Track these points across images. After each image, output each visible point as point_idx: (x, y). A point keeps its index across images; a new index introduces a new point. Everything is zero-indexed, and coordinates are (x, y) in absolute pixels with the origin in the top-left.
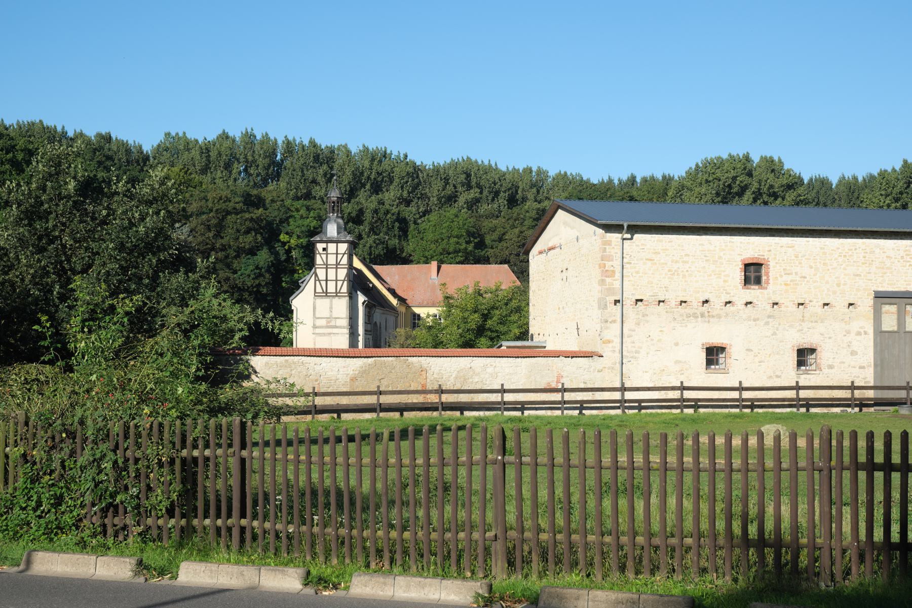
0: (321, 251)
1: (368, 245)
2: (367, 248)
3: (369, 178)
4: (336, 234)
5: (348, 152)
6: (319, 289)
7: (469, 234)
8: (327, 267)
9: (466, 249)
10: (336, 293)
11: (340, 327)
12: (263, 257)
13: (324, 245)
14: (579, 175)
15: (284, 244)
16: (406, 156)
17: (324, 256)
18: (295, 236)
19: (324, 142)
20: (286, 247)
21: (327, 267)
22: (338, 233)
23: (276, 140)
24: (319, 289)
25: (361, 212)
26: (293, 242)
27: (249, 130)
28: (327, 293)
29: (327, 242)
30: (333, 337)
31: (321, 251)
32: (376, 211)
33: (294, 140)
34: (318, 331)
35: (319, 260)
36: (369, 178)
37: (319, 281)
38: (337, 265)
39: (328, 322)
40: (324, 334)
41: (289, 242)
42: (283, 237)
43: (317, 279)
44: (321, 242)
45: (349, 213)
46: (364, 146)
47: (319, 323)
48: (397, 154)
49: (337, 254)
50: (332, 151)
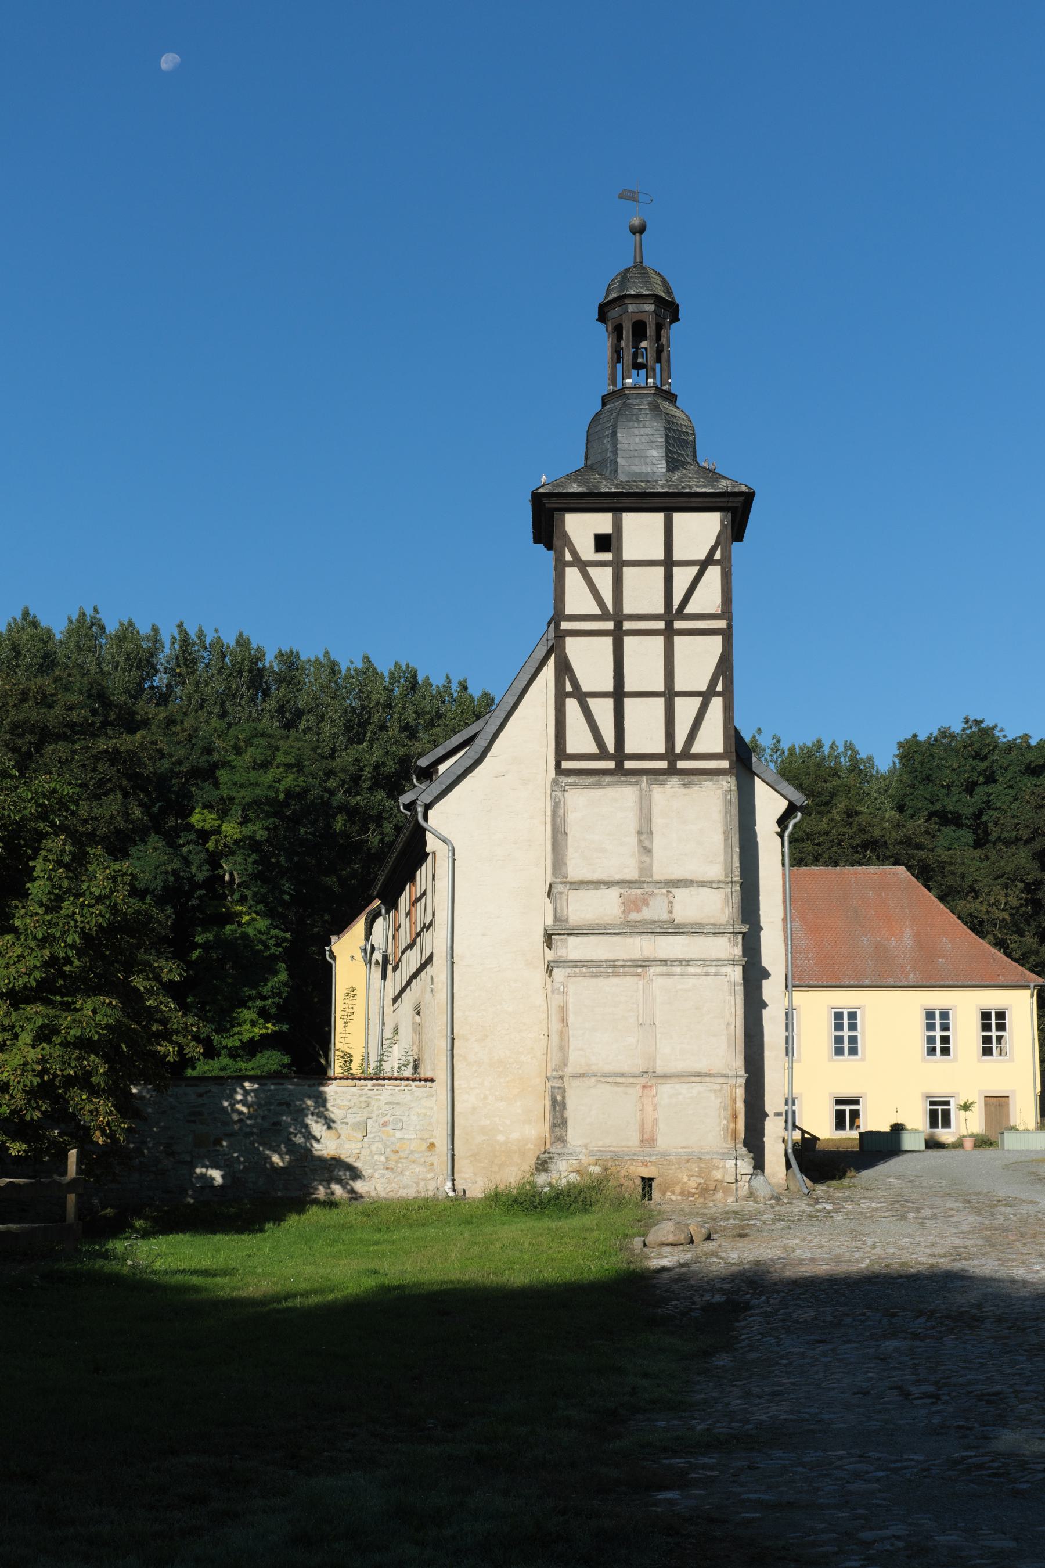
0: (586, 550)
4: (662, 467)
5: (333, 667)
6: (580, 740)
8: (618, 626)
10: (670, 755)
11: (698, 930)
12: (149, 861)
13: (603, 522)
14: (849, 746)
15: (204, 835)
17: (603, 578)
18: (237, 813)
19: (271, 647)
20: (210, 845)
21: (618, 626)
23: (155, 630)
24: (580, 740)
26: (230, 829)
27: (89, 612)
28: (620, 755)
30: (659, 981)
31: (586, 550)
33: (201, 635)
34: (575, 948)
38: (671, 621)
39: (631, 905)
40: (610, 967)
41: (217, 831)
42: (199, 818)
44: (590, 502)
45: (377, 767)
46: (367, 659)
47: (582, 907)
49: (669, 563)
50: (290, 661)
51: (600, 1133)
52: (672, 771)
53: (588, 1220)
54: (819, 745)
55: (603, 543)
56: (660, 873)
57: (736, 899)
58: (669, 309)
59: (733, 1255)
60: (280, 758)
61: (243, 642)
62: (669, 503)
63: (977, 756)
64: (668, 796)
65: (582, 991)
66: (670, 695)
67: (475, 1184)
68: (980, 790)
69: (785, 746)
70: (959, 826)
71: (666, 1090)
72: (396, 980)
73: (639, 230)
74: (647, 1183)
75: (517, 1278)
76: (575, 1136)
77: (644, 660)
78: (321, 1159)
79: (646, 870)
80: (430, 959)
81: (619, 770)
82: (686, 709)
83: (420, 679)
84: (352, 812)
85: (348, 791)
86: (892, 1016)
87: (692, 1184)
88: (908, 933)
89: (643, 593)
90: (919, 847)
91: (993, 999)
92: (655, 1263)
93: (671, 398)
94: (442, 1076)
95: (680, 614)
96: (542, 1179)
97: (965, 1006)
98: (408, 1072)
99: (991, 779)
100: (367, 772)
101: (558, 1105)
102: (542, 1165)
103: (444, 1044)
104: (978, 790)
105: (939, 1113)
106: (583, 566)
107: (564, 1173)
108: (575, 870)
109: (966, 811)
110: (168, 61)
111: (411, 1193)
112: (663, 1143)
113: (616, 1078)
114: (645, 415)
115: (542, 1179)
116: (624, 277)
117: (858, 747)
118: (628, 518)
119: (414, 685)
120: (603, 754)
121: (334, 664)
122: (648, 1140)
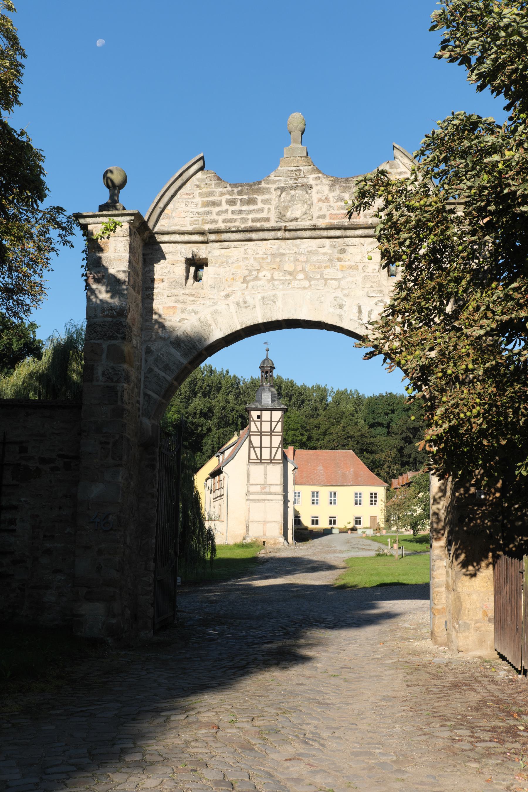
0: (255, 418)
1: (217, 436)
2: (216, 439)
3: (201, 387)
4: (270, 402)
6: (253, 456)
7: (303, 427)
8: (261, 434)
9: (301, 440)
10: (270, 459)
11: (275, 494)
13: (258, 413)
14: (356, 391)
16: (228, 372)
17: (258, 424)
21: (261, 434)
24: (253, 456)
25: (210, 410)
28: (261, 459)
29: (261, 410)
32: (224, 408)
34: (251, 497)
35: (253, 428)
36: (201, 387)
37: (254, 448)
38: (271, 433)
39: (263, 489)
40: (258, 501)
43: (251, 445)
44: (256, 409)
45: (201, 410)
47: (253, 489)
48: (220, 370)
49: (271, 421)
51: (256, 533)
52: (271, 463)
53: (252, 549)
54: (346, 390)
55: (259, 417)
56: (268, 483)
60: (173, 409)
62: (272, 410)
63: (389, 405)
64: (270, 467)
65: (252, 505)
67: (231, 542)
68: (390, 415)
69: (335, 390)
70: (383, 427)
71: (268, 525)
73: (268, 351)
74: (264, 542)
75: (238, 557)
76: (251, 533)
79: (265, 482)
80: (223, 495)
81: (261, 462)
82: (274, 451)
83: (213, 369)
84: (193, 423)
85: (193, 417)
86: (346, 494)
87: (273, 543)
88: (352, 470)
89: (266, 427)
90: (366, 437)
91: (374, 490)
92: (260, 556)
94: (225, 520)
95: (273, 432)
96: (244, 541)
97: (366, 491)
99: (393, 411)
100: (198, 412)
101: (247, 527)
102: (244, 539)
103: (226, 514)
104: (389, 415)
105: (358, 521)
106: (254, 421)
107: (248, 540)
108: (252, 482)
109: (384, 422)
110: (100, 43)
114: (268, 391)
115: (244, 541)
116: (264, 361)
117: (359, 392)
120: (258, 459)
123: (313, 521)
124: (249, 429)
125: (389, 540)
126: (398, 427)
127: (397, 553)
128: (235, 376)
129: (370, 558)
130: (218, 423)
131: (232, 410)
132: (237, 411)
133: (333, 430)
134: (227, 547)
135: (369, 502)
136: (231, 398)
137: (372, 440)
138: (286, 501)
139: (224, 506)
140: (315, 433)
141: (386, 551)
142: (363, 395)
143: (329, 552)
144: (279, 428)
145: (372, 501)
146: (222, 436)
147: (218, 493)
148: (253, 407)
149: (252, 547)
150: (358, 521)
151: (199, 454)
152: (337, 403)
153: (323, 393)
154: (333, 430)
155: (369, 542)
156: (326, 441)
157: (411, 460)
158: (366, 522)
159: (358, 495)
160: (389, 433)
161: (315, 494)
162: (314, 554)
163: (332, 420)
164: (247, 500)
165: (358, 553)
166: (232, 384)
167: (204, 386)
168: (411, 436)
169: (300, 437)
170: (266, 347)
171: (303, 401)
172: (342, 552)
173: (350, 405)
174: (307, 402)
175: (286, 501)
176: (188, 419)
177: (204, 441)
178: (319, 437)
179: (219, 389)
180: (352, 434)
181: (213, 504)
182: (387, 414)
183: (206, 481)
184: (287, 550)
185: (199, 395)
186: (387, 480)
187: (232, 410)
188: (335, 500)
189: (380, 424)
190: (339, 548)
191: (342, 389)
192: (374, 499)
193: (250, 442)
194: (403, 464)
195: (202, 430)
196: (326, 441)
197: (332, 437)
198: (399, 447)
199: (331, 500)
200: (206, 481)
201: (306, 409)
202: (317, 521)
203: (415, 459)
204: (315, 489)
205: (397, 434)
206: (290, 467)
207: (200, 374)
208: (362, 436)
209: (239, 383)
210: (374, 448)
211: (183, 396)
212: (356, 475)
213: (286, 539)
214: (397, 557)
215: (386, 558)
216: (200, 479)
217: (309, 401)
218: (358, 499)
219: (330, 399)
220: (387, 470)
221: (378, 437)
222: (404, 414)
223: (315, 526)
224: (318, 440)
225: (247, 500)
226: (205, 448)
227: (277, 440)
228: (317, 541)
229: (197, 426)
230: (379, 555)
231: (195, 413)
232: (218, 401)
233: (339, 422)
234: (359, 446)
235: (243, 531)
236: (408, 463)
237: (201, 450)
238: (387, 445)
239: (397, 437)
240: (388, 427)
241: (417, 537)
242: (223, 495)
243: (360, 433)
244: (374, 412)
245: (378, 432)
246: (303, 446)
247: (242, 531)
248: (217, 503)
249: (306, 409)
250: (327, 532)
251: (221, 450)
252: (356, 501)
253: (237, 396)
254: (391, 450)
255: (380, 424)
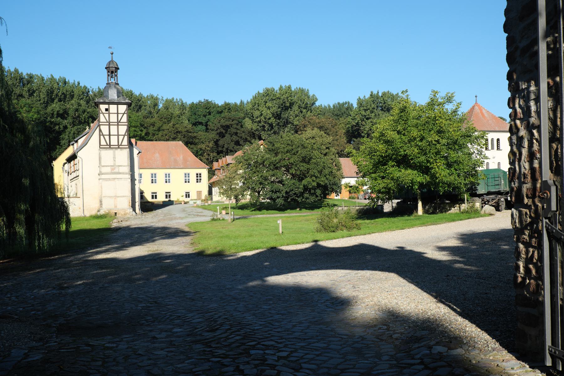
0: (104, 111)
1: (72, 132)
3: (57, 95)
6: (103, 143)
8: (109, 124)
9: (141, 135)
10: (118, 145)
11: (123, 173)
14: (181, 100)
17: (107, 116)
21: (109, 124)
22: (118, 97)
28: (110, 145)
29: (109, 103)
32: (77, 110)
34: (103, 176)
35: (102, 119)
36: (57, 95)
37: (103, 135)
38: (118, 123)
39: (113, 169)
40: (109, 179)
44: (104, 103)
45: (58, 111)
46: (52, 75)
47: (104, 170)
49: (118, 113)
50: (31, 77)
51: (108, 206)
52: (119, 148)
53: (106, 219)
54: (173, 99)
55: (107, 110)
56: (117, 165)
57: (129, 168)
58: (117, 69)
59: (124, 224)
60: (33, 110)
61: (16, 71)
62: (118, 104)
63: (206, 108)
66: (118, 135)
67: (88, 214)
68: (208, 117)
69: (164, 99)
71: (118, 199)
72: (71, 177)
73: (112, 54)
74: (116, 213)
75: (95, 227)
76: (104, 206)
77: (114, 129)
78: (368, 326)
79: (115, 164)
80: (78, 176)
81: (110, 147)
83: (67, 81)
84: (52, 123)
85: (51, 118)
86: (177, 175)
87: (123, 213)
88: (181, 157)
89: (113, 118)
90: (191, 132)
91: (199, 171)
93: (118, 84)
94: (81, 197)
97: (193, 173)
98: (75, 196)
99: (210, 113)
100: (55, 113)
101: (101, 202)
102: (99, 211)
105: (188, 195)
106: (103, 114)
107: (102, 212)
108: (103, 164)
111: (77, 216)
112: (118, 207)
113: (110, 197)
114: (114, 88)
115: (99, 213)
118: (110, 105)
119: (65, 83)
120: (107, 145)
121: (43, 77)
122: (116, 207)
123: (153, 196)
124: (99, 121)
125: (218, 208)
126: (214, 125)
127: (229, 218)
128: (85, 86)
129: (207, 222)
130: (73, 122)
131: (84, 111)
132: (88, 113)
133: (165, 127)
134: (79, 219)
135: (196, 181)
136: (82, 102)
137: (195, 134)
138: (133, 180)
139: (80, 185)
140: (151, 130)
141: (219, 216)
142: (186, 103)
143: (171, 219)
144: (125, 119)
145: (197, 179)
146: (76, 132)
147: (74, 175)
148: (101, 101)
149: (106, 217)
150: (188, 195)
151: (58, 147)
152: (167, 108)
153: (156, 101)
154: (165, 127)
155: (200, 210)
156: (160, 136)
157: (224, 149)
158: (193, 196)
159: (187, 175)
160: (207, 129)
161: (154, 176)
162: (159, 221)
163: (164, 120)
164: (99, 179)
165: (194, 219)
166: (83, 93)
167: (60, 94)
168: (224, 131)
169: (140, 132)
170: (111, 51)
171: (140, 107)
172: (181, 218)
173: (176, 109)
174: (143, 107)
175: (133, 180)
176: (47, 118)
177: (61, 136)
178: (154, 132)
179: (72, 97)
180: (180, 130)
181: (70, 184)
182: (205, 116)
183: (64, 166)
184: (135, 218)
185: (56, 101)
186: (209, 163)
187: (84, 111)
188: (169, 180)
189: (201, 123)
190: (178, 215)
191: (170, 98)
192: (199, 178)
193: (100, 131)
194: (218, 153)
195: (59, 128)
196: (160, 136)
197: (164, 133)
198: (215, 140)
199: (166, 180)
200: (64, 166)
201: (143, 112)
202: (156, 196)
203: (227, 149)
204: (153, 171)
205: (213, 130)
206: (136, 151)
207: (56, 84)
208: (187, 131)
209: (89, 92)
210: (197, 141)
211: (42, 102)
212: (185, 160)
213: (134, 210)
214: (230, 221)
215: (220, 221)
216: (58, 164)
217: (145, 106)
218: (187, 178)
219: (161, 106)
220: (207, 157)
221: (200, 133)
222: (218, 115)
223: (154, 200)
224: (154, 135)
225: (99, 179)
226: (62, 142)
227: (123, 129)
228: (159, 211)
229: (56, 124)
230: (213, 220)
231: (53, 114)
232: (71, 105)
233: (169, 121)
234: (185, 139)
235: (97, 205)
236: (222, 152)
237: (59, 144)
238: (207, 139)
239: (213, 132)
240: (206, 125)
241: (238, 205)
242: (78, 176)
243: (186, 130)
244: (195, 114)
245: (198, 129)
246: (142, 139)
247: (96, 205)
248: (74, 183)
249: (143, 112)
250: (165, 204)
251: (75, 140)
252: (186, 179)
253: (88, 102)
254: (209, 142)
255: (201, 123)
